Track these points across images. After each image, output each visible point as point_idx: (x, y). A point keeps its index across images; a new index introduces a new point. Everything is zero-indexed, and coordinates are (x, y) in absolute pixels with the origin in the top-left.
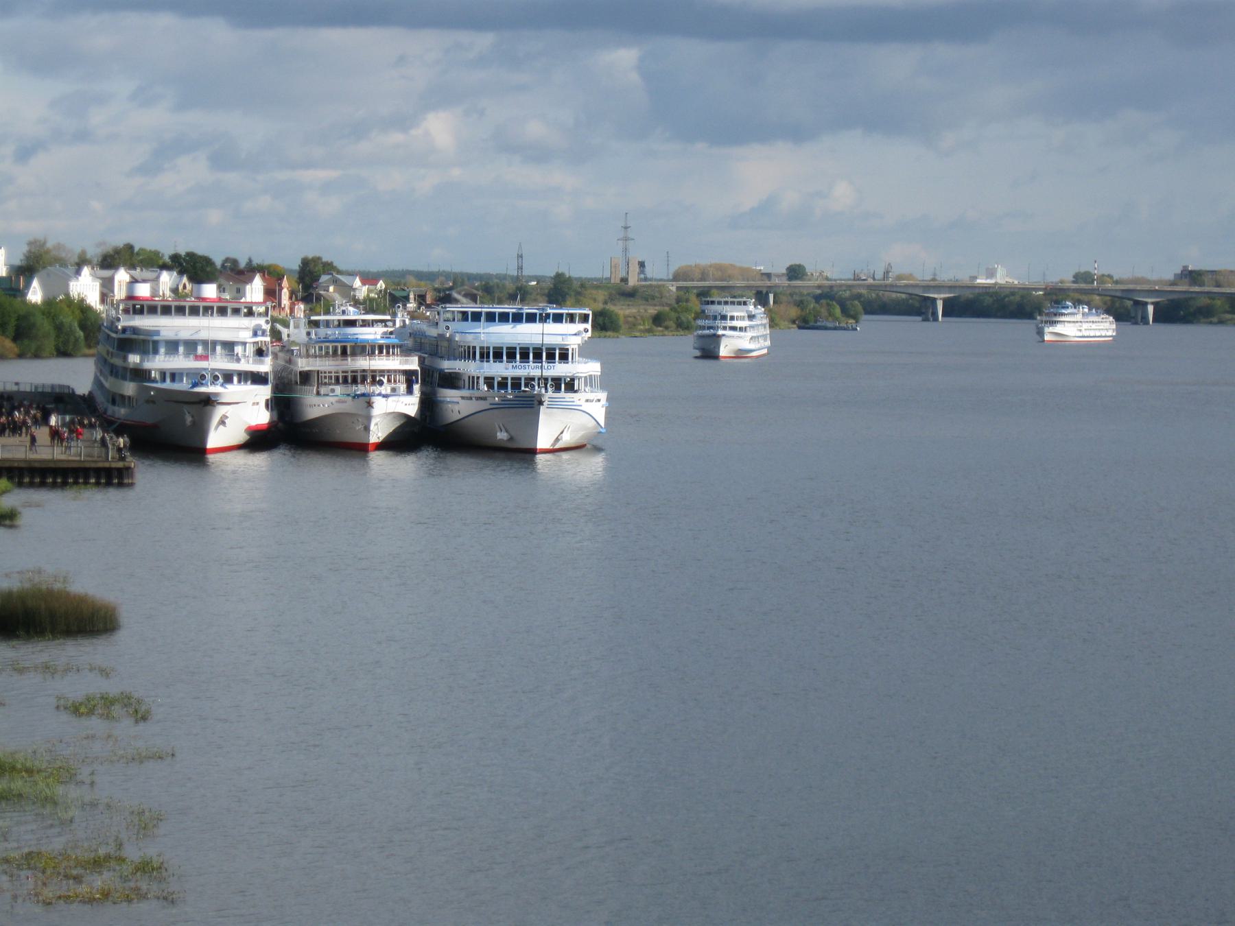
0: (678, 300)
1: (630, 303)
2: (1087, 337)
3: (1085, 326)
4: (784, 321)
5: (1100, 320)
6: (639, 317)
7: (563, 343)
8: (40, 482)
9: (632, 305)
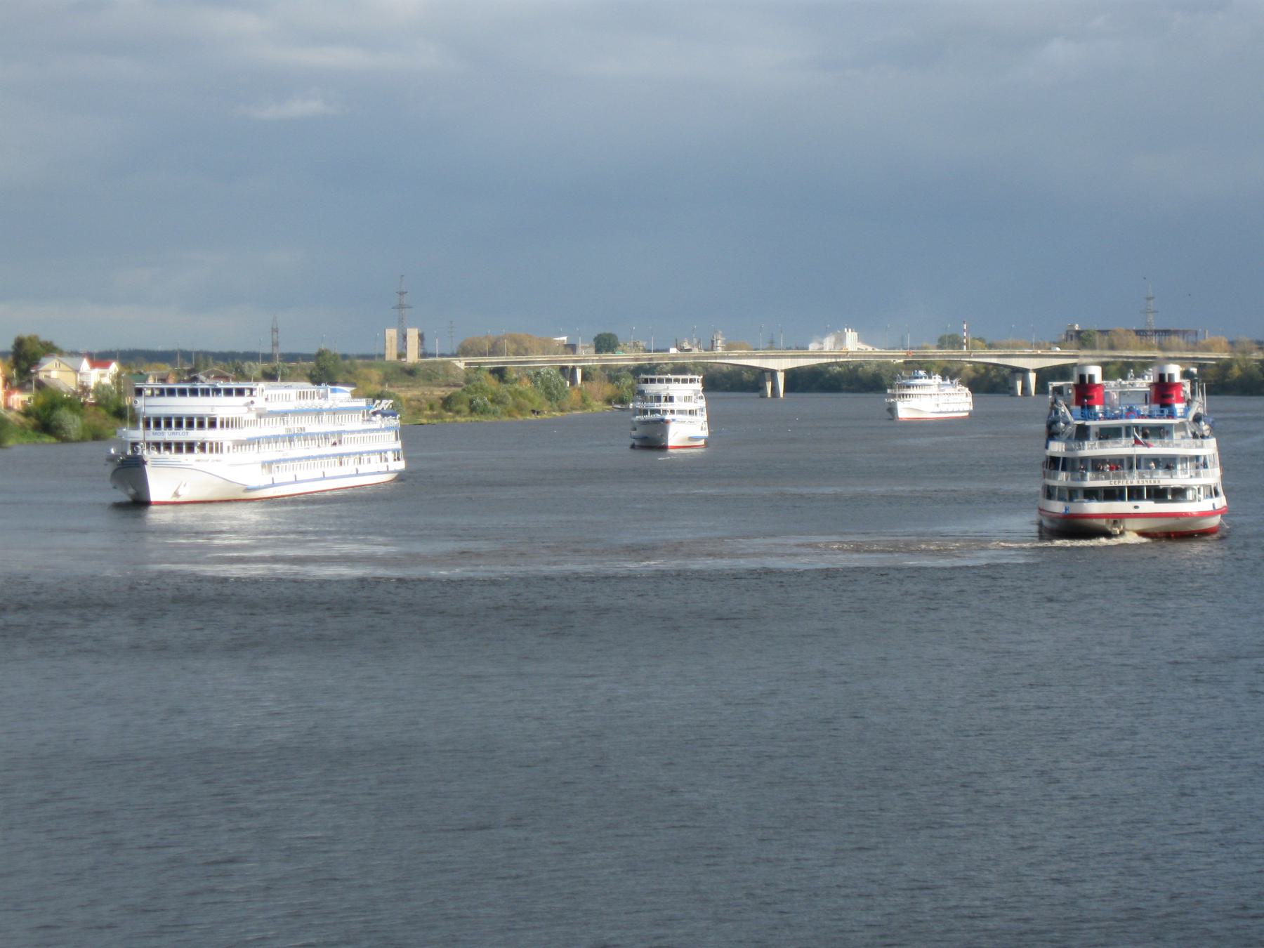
0: (468, 381)
1: (410, 384)
2: (959, 412)
3: (942, 399)
4: (540, 403)
5: (957, 392)
6: (424, 401)
7: (211, 413)
8: (113, 455)
9: (413, 386)
